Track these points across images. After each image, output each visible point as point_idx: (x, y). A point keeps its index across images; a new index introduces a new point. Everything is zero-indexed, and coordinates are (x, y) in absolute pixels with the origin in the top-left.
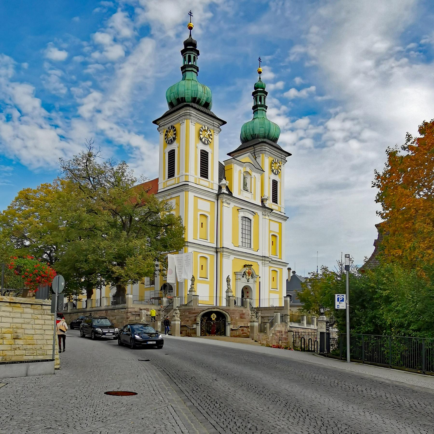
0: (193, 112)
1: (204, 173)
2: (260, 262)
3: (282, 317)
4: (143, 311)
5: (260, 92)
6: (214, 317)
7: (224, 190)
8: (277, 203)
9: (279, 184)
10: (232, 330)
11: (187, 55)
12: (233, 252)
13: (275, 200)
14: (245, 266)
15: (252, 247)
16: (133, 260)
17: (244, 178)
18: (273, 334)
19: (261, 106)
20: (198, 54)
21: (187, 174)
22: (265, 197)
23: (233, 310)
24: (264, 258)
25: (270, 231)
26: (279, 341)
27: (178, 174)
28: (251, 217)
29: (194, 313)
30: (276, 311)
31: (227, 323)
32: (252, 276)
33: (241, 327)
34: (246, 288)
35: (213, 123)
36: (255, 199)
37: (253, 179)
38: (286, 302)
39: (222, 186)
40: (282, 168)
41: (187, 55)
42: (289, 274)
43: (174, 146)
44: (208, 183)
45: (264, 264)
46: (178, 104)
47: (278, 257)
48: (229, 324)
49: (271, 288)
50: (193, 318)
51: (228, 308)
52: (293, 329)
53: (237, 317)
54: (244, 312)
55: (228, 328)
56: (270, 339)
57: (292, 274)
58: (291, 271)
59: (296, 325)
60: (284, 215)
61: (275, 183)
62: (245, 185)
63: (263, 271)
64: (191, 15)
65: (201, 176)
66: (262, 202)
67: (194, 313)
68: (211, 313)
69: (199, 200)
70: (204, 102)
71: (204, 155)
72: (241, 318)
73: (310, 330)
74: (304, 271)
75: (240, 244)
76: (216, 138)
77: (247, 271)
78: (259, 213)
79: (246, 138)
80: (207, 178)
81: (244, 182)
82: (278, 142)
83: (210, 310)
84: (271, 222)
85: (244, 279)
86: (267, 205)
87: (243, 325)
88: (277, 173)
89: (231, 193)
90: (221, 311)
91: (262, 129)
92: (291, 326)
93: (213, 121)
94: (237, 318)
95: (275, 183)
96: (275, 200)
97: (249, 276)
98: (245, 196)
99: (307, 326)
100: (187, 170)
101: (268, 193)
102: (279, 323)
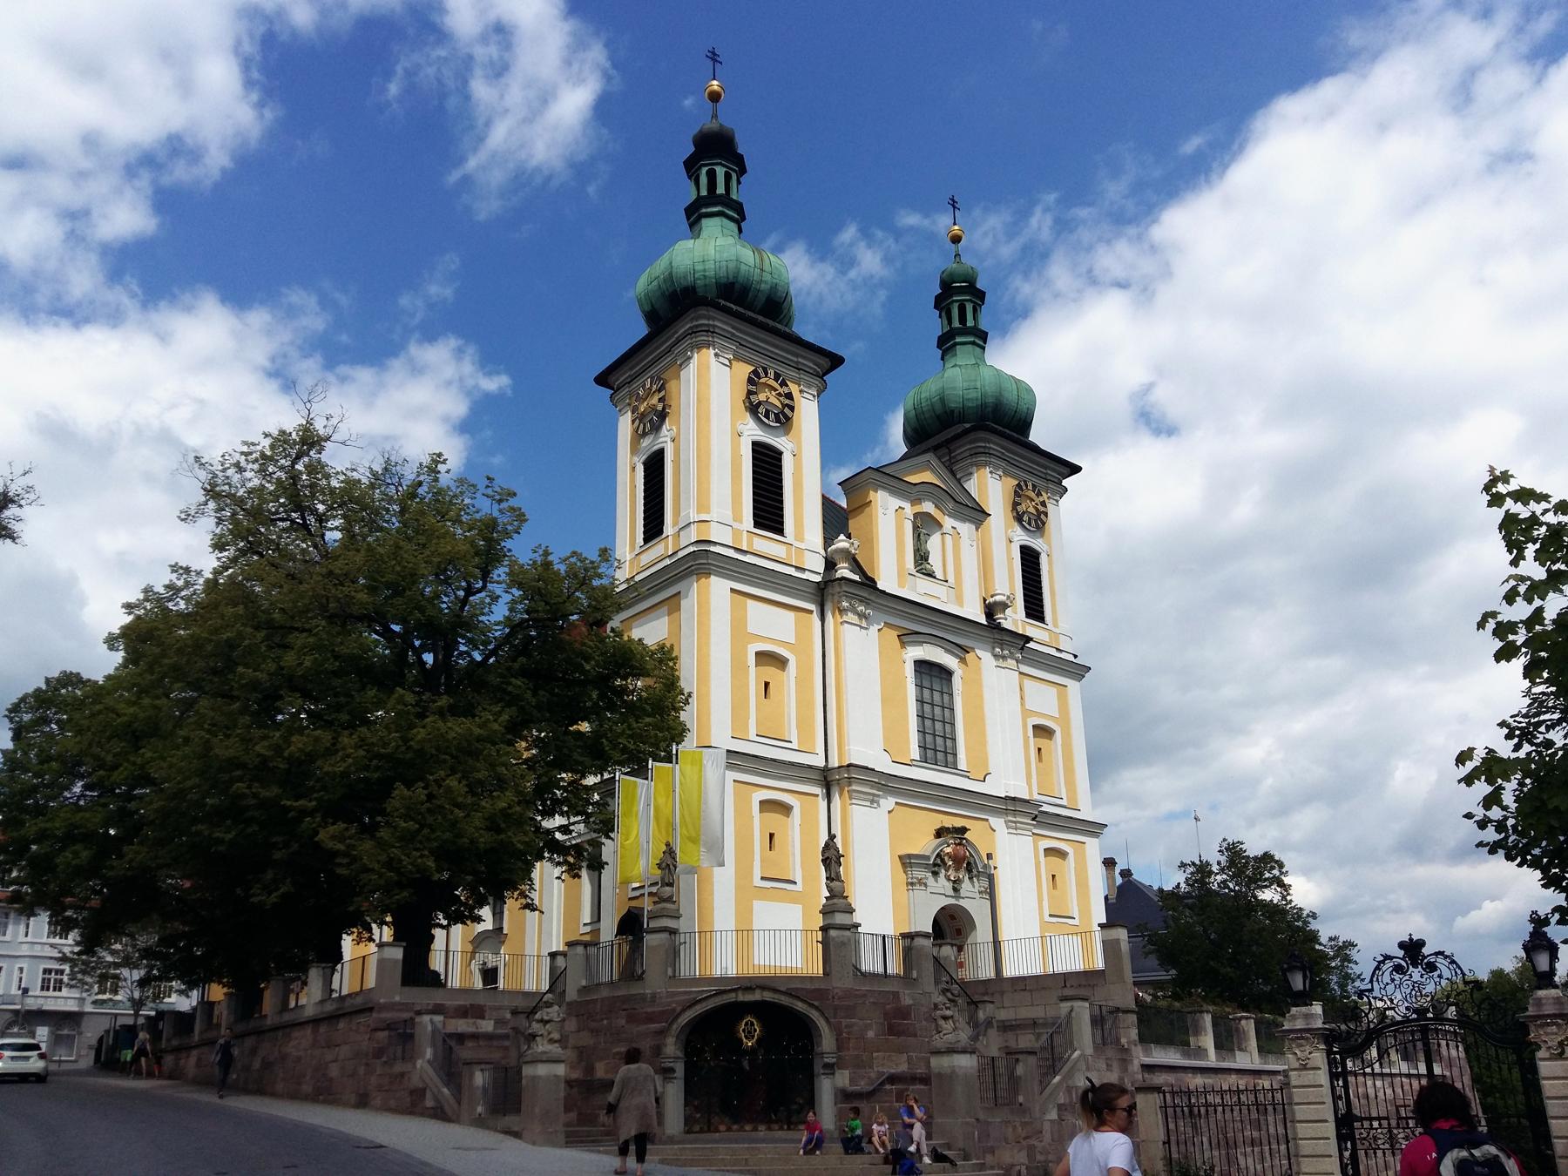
0: (721, 323)
1: (769, 514)
2: (997, 822)
3: (1098, 1021)
4: (426, 1018)
5: (960, 291)
6: (749, 1033)
7: (844, 571)
8: (1041, 619)
9: (1043, 560)
10: (844, 1096)
11: (704, 170)
12: (886, 784)
13: (1035, 609)
14: (939, 833)
15: (962, 765)
16: (423, 797)
17: (920, 539)
18: (1061, 1107)
19: (965, 331)
20: (742, 171)
21: (704, 517)
22: (998, 598)
23: (849, 994)
24: (1011, 806)
25: (1026, 713)
27: (675, 523)
28: (949, 661)
29: (650, 1018)
30: (1068, 992)
31: (818, 1068)
32: (969, 870)
33: (892, 1079)
34: (953, 917)
36: (959, 600)
37: (948, 538)
38: (1110, 948)
39: (837, 557)
40: (1050, 508)
41: (704, 170)
42: (1110, 878)
43: (665, 439)
44: (784, 547)
45: (1013, 827)
46: (680, 313)
47: (1064, 802)
48: (827, 1066)
49: (1046, 913)
52: (1160, 1079)
53: (868, 1027)
54: (907, 1001)
55: (826, 1089)
56: (1047, 1137)
57: (1119, 880)
58: (1117, 871)
59: (1171, 1057)
60: (1071, 658)
61: (1030, 560)
62: (921, 557)
63: (1012, 852)
64: (715, 61)
65: (757, 525)
66: (991, 610)
67: (650, 1018)
68: (734, 1012)
69: (750, 603)
70: (762, 298)
71: (767, 465)
72: (892, 1030)
73: (1232, 1081)
74: (1162, 873)
75: (915, 753)
76: (807, 411)
77: (948, 850)
78: (984, 657)
80: (780, 532)
81: (917, 551)
82: (1034, 437)
83: (731, 997)
84: (1027, 682)
85: (943, 885)
86: (1006, 624)
87: (903, 1068)
88: (1036, 522)
89: (873, 581)
90: (785, 1000)
91: (973, 394)
92: (1148, 1060)
93: (797, 356)
94: (871, 1034)
95: (1030, 560)
96: (1035, 609)
97: (957, 870)
98: (920, 591)
99: (1220, 1057)
100: (703, 506)
101: (1009, 584)
102: (1089, 1051)
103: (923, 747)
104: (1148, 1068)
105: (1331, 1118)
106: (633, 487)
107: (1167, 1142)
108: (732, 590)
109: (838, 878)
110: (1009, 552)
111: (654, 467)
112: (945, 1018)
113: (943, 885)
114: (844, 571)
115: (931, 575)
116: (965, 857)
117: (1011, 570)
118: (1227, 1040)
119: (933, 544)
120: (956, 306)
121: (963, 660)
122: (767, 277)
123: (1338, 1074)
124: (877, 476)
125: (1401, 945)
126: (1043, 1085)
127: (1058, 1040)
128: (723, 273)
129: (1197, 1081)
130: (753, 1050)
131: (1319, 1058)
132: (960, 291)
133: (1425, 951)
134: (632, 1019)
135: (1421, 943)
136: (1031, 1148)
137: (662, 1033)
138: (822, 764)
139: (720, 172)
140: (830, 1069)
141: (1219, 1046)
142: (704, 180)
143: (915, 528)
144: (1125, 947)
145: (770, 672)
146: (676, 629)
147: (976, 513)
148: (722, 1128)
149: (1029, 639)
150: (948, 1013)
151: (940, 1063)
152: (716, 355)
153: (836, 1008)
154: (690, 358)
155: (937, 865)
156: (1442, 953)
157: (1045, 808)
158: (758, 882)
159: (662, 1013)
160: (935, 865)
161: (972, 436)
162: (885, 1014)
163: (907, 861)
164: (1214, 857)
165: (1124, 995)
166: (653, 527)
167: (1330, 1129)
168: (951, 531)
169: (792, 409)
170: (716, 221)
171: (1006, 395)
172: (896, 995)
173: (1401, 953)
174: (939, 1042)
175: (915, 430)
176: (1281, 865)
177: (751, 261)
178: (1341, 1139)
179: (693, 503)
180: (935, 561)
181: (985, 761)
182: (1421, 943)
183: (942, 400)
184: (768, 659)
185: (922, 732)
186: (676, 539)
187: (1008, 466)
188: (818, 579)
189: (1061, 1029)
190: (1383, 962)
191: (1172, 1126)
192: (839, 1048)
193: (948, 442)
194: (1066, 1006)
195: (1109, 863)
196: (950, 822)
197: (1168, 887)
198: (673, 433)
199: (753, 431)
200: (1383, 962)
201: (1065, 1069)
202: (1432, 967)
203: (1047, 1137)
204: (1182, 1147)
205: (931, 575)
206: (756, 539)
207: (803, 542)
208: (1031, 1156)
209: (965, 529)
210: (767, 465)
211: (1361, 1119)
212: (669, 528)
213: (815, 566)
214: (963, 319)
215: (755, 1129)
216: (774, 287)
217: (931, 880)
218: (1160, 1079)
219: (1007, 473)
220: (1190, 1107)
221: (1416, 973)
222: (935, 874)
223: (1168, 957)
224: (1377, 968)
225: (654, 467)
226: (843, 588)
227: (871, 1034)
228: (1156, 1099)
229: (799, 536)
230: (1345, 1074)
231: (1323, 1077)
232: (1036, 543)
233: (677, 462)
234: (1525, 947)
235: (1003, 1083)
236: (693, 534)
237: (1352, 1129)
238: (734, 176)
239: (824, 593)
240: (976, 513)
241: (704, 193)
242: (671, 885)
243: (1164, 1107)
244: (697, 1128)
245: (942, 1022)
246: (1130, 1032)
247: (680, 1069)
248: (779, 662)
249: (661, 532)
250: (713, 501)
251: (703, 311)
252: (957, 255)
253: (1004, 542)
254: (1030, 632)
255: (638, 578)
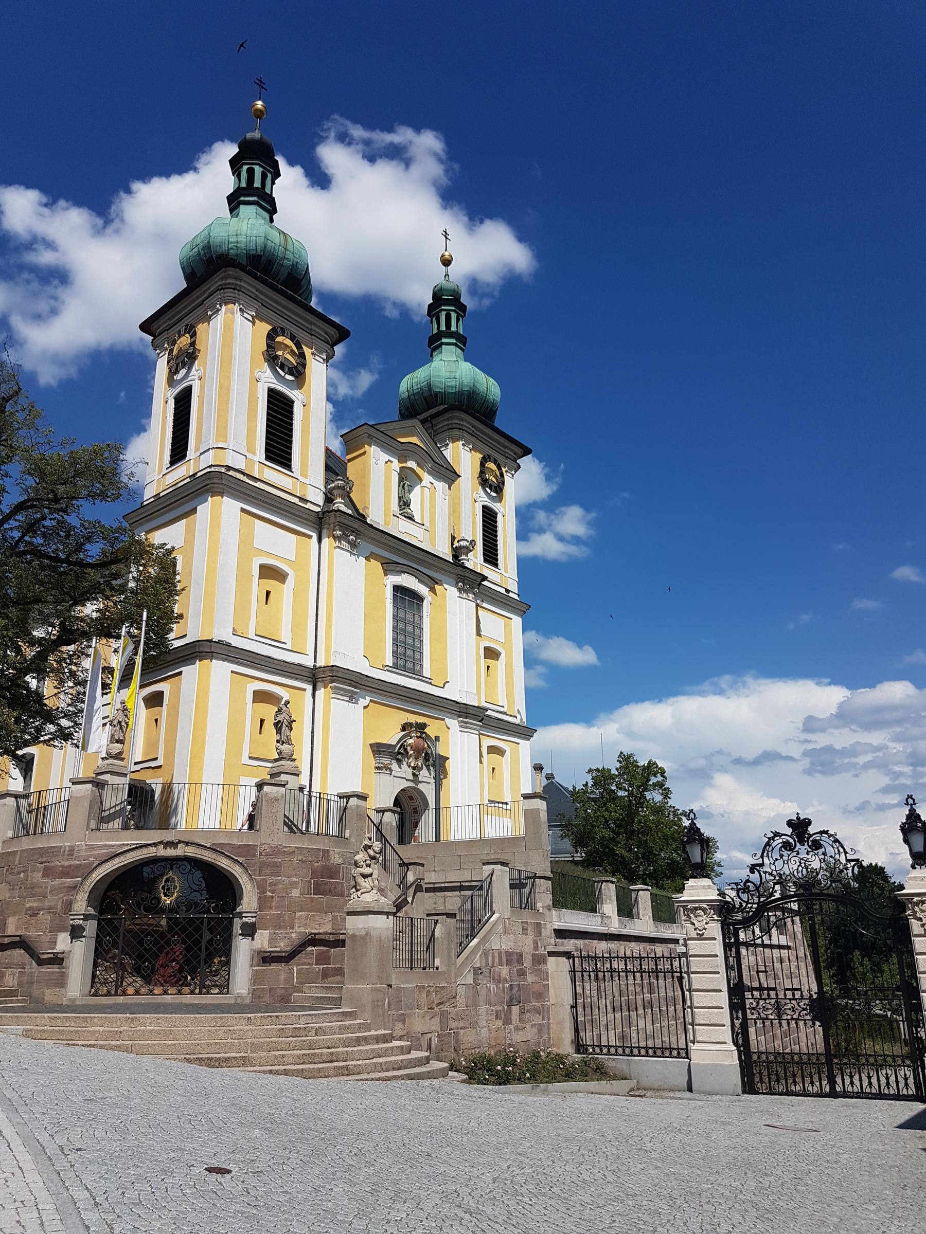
0: (247, 283)
1: (279, 448)
2: (453, 723)
3: (516, 885)
9: (499, 518)
10: (266, 958)
11: (245, 167)
15: (426, 673)
18: (477, 971)
23: (276, 851)
26: (510, 1005)
27: (197, 450)
28: (423, 590)
29: (66, 872)
33: (313, 941)
34: (411, 798)
35: (311, 329)
36: (433, 541)
38: (530, 815)
41: (245, 167)
45: (464, 725)
47: (505, 710)
50: (57, 901)
51: (250, 839)
53: (294, 885)
54: (336, 860)
55: (243, 950)
57: (545, 782)
62: (404, 504)
63: (458, 743)
65: (268, 458)
66: (457, 552)
67: (66, 872)
71: (280, 412)
75: (389, 661)
76: (317, 370)
77: (411, 741)
79: (412, 405)
80: (288, 466)
84: (480, 611)
90: (208, 856)
91: (452, 383)
92: (558, 925)
93: (311, 323)
98: (402, 529)
100: (222, 432)
101: (473, 530)
103: (395, 654)
104: (561, 934)
105: (724, 988)
106: (165, 417)
107: (574, 1006)
108: (243, 510)
109: (288, 741)
110: (473, 507)
111: (183, 402)
112: (365, 876)
113: (407, 772)
114: (340, 504)
115: (411, 518)
116: (424, 748)
117: (474, 523)
118: (626, 909)
119: (415, 496)
120: (444, 313)
121: (432, 590)
122: (289, 255)
123: (732, 946)
124: (372, 432)
125: (790, 823)
126: (462, 947)
127: (478, 903)
128: (252, 246)
129: (602, 947)
130: (172, 909)
131: (715, 929)
132: (448, 302)
133: (812, 829)
134: (47, 872)
135: (807, 823)
136: (444, 1015)
137: (74, 888)
138: (310, 663)
139: (258, 170)
140: (250, 931)
141: (621, 913)
142: (244, 175)
143: (401, 480)
144: (544, 816)
145: (271, 584)
146: (190, 534)
147: (449, 474)
148: (130, 990)
149: (485, 578)
150: (367, 871)
151: (354, 924)
152: (241, 310)
153: (262, 865)
154: (218, 310)
155: (398, 753)
156: (826, 832)
157: (489, 713)
158: (245, 760)
159: (78, 867)
160: (399, 753)
161: (447, 415)
162: (314, 873)
163: (378, 749)
164: (613, 765)
165: (541, 864)
166: (179, 452)
167: (723, 999)
168: (429, 485)
169: (304, 366)
170: (253, 208)
171: (478, 386)
172: (326, 853)
173: (789, 831)
174: (352, 905)
175: (407, 409)
176: (663, 773)
177: (277, 241)
178: (733, 1007)
179: (213, 431)
180: (415, 508)
181: (445, 672)
182: (807, 823)
183: (429, 385)
184: (269, 572)
185: (395, 629)
186: (197, 461)
187: (475, 440)
188: (318, 509)
189: (478, 890)
190: (773, 838)
191: (579, 990)
192: (260, 908)
193: (433, 417)
194: (487, 869)
195: (538, 768)
196: (413, 719)
197: (579, 787)
198: (200, 373)
199: (268, 379)
200: (773, 838)
201: (482, 934)
202: (816, 845)
203: (461, 1001)
204: (588, 1010)
205: (411, 518)
206: (266, 469)
207: (307, 480)
208: (443, 1024)
209: (441, 486)
210: (280, 412)
211: (752, 989)
212: (191, 453)
213: (317, 498)
214: (448, 324)
215: (165, 993)
216: (295, 266)
217: (394, 766)
218: (569, 945)
219: (475, 449)
220: (596, 971)
221: (803, 849)
222: (399, 762)
223: (580, 841)
224: (768, 844)
225: (183, 402)
226: (339, 520)
227: (296, 893)
228: (564, 962)
229: (304, 474)
230: (738, 944)
231: (718, 947)
232: (496, 506)
233: (201, 397)
234: (903, 828)
235: (420, 948)
236: (209, 459)
237: (743, 999)
238: (269, 176)
239: (322, 522)
240: (449, 474)
241: (244, 185)
242: (121, 742)
243: (573, 971)
244: (104, 990)
245: (360, 880)
246: (544, 895)
247: (91, 927)
248: (279, 575)
249: (185, 456)
250: (231, 433)
251: (231, 271)
252: (447, 275)
253: (470, 501)
254: (486, 572)
255: (162, 495)
